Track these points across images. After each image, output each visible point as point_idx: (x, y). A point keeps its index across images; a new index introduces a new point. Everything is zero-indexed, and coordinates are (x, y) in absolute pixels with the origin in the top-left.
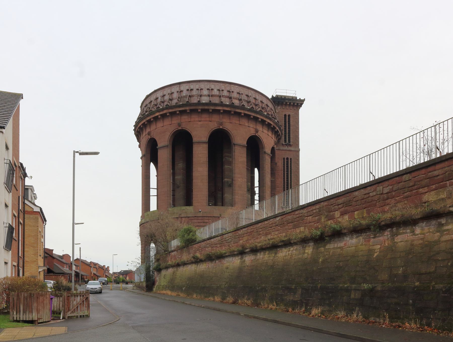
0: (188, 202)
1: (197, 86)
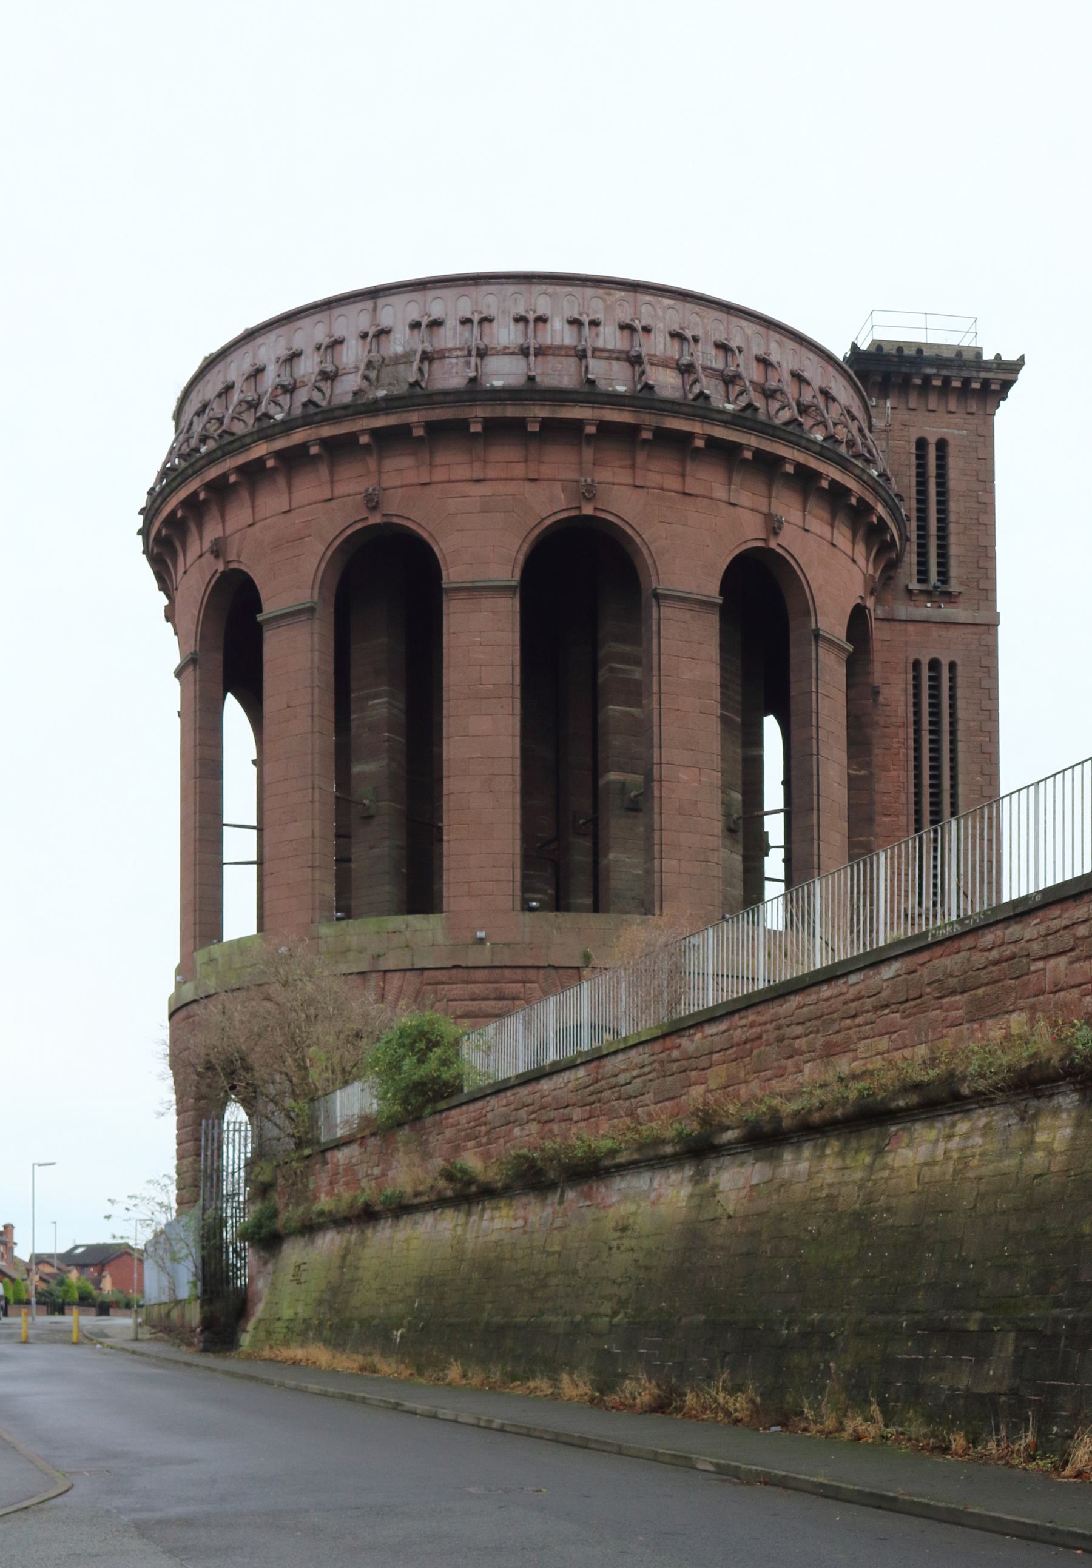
0: (420, 891)
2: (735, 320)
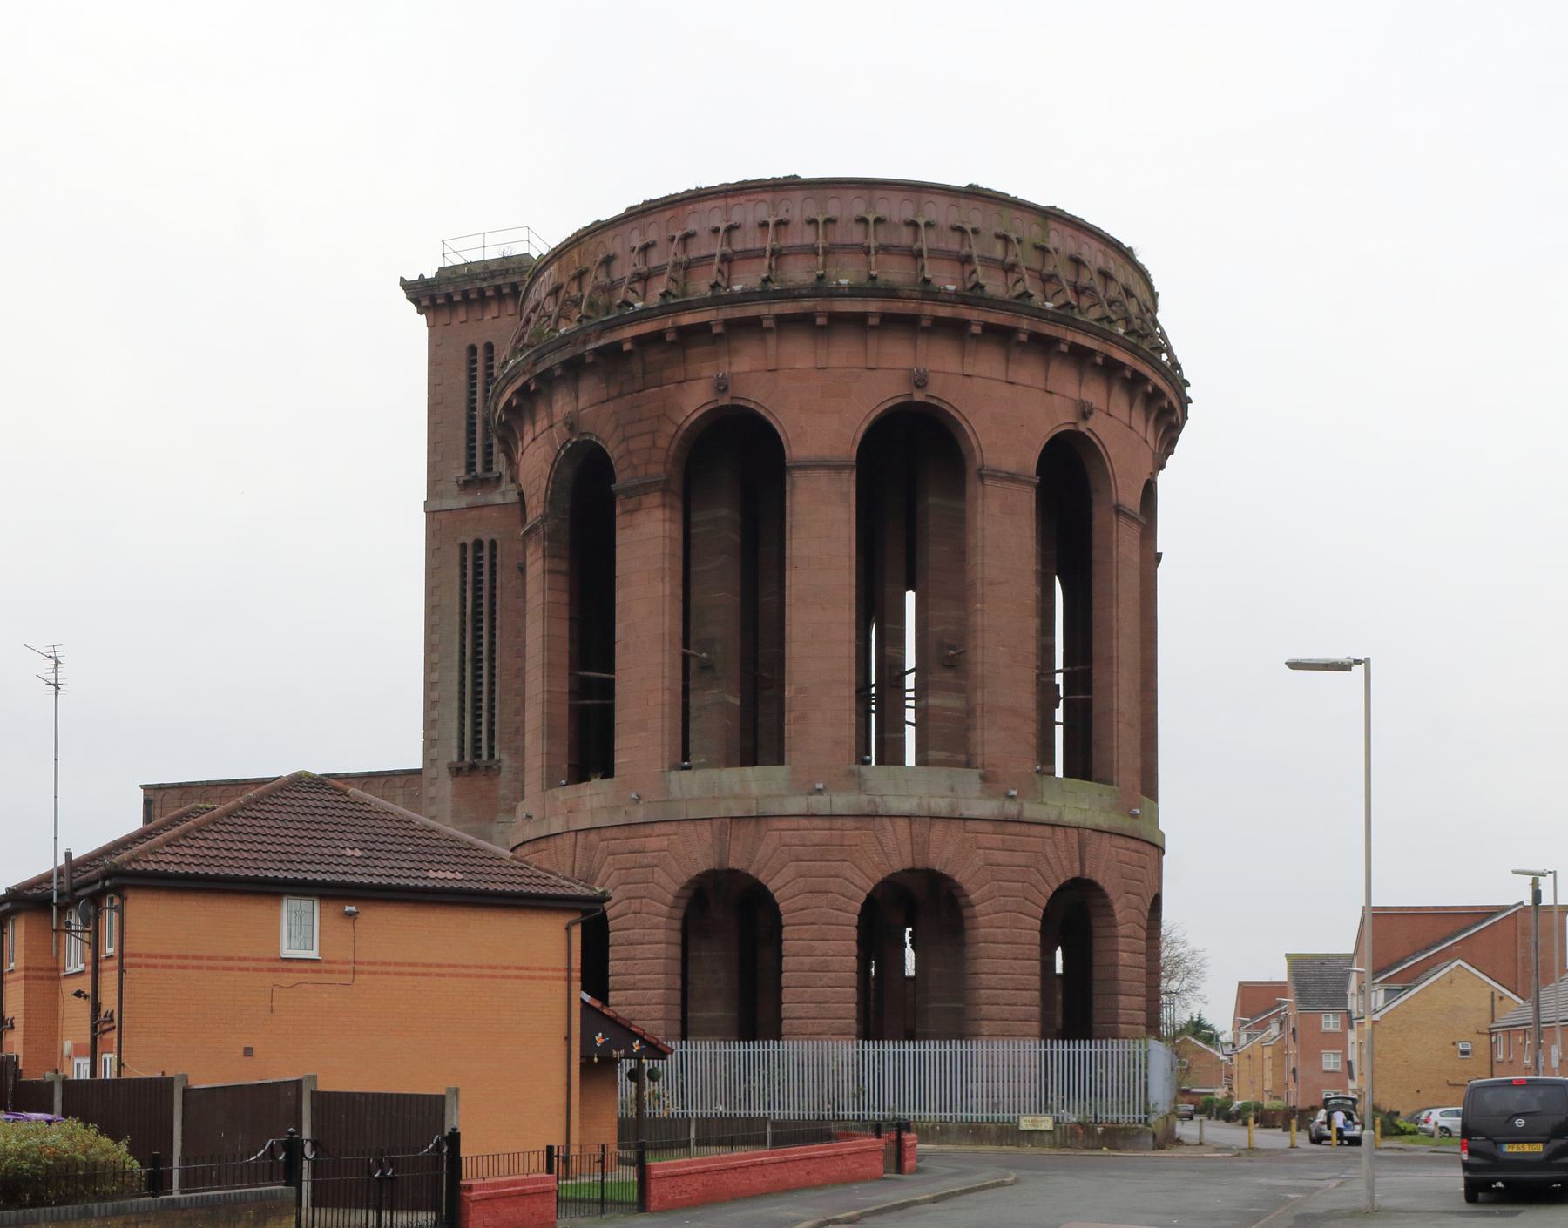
0: (758, 739)
1: (762, 210)
2: (1082, 237)
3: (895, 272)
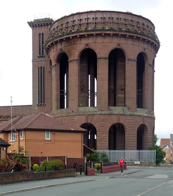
1: (93, 16)
3: (115, 27)
